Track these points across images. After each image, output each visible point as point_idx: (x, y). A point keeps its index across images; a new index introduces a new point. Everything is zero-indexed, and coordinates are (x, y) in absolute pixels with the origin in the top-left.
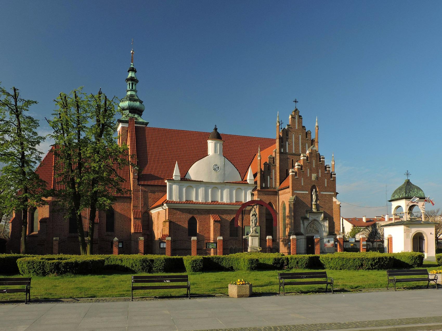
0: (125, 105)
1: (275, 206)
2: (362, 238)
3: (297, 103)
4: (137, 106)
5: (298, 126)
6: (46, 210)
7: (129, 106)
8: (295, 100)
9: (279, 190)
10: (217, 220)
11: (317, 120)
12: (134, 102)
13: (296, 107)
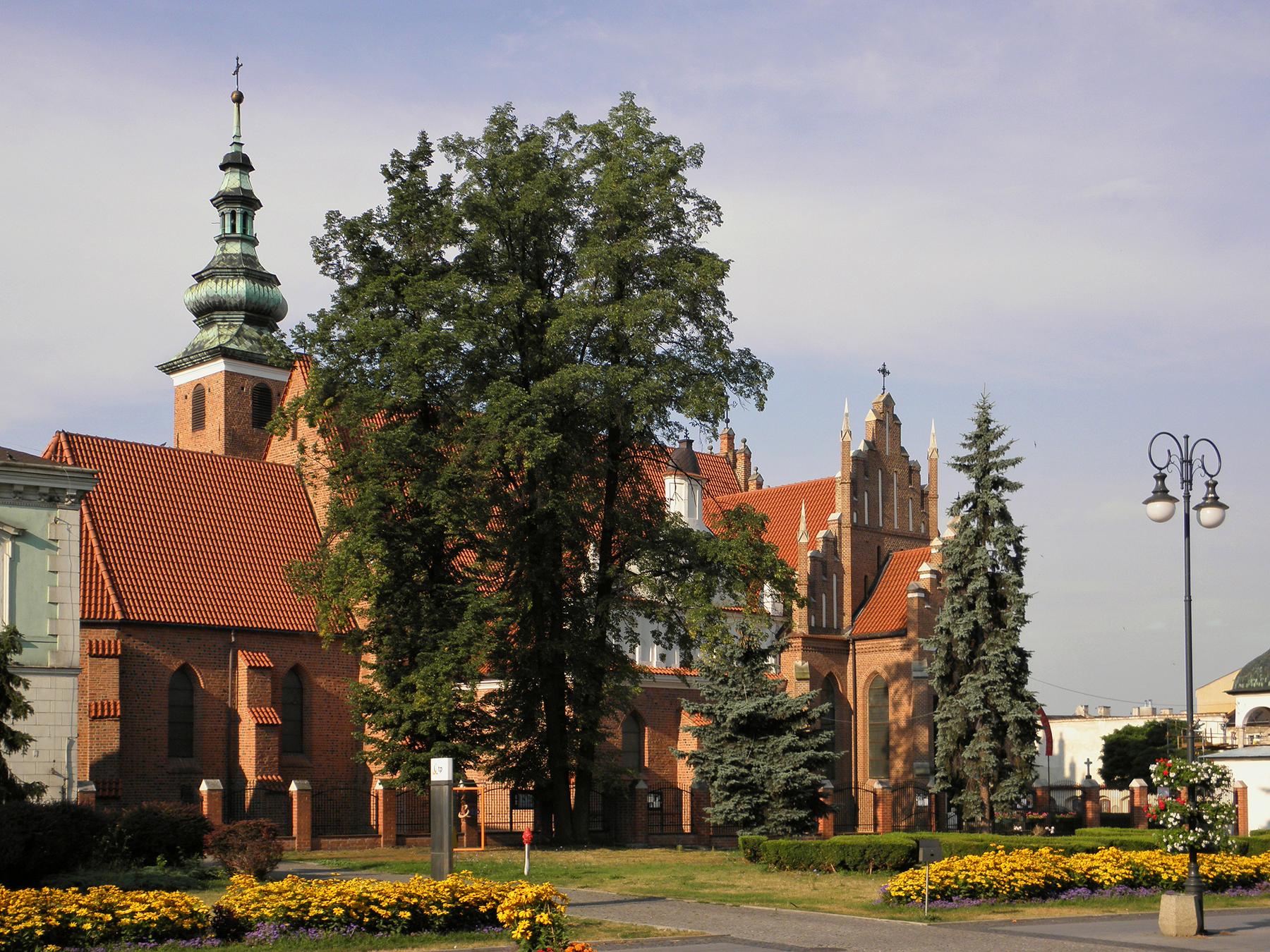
0: (230, 293)
1: (842, 687)
2: (1141, 787)
3: (887, 377)
4: (274, 301)
5: (892, 446)
6: (105, 675)
7: (249, 300)
8: (881, 367)
9: (857, 640)
10: (268, 709)
11: (933, 431)
12: (265, 288)
13: (884, 389)
